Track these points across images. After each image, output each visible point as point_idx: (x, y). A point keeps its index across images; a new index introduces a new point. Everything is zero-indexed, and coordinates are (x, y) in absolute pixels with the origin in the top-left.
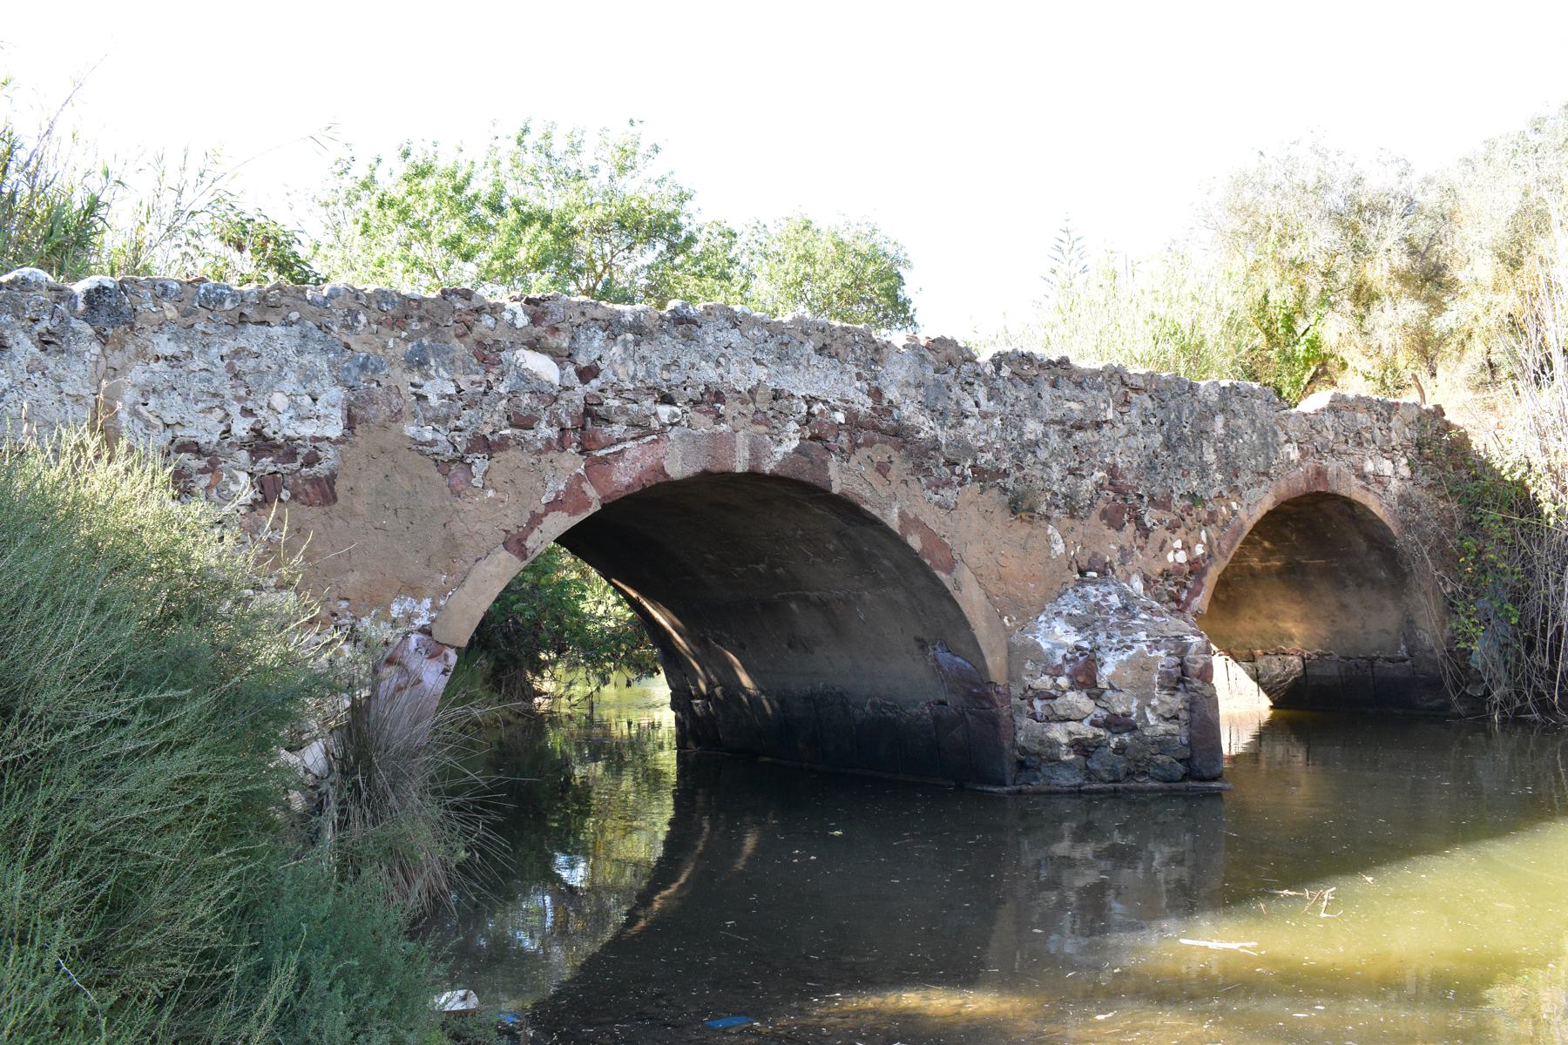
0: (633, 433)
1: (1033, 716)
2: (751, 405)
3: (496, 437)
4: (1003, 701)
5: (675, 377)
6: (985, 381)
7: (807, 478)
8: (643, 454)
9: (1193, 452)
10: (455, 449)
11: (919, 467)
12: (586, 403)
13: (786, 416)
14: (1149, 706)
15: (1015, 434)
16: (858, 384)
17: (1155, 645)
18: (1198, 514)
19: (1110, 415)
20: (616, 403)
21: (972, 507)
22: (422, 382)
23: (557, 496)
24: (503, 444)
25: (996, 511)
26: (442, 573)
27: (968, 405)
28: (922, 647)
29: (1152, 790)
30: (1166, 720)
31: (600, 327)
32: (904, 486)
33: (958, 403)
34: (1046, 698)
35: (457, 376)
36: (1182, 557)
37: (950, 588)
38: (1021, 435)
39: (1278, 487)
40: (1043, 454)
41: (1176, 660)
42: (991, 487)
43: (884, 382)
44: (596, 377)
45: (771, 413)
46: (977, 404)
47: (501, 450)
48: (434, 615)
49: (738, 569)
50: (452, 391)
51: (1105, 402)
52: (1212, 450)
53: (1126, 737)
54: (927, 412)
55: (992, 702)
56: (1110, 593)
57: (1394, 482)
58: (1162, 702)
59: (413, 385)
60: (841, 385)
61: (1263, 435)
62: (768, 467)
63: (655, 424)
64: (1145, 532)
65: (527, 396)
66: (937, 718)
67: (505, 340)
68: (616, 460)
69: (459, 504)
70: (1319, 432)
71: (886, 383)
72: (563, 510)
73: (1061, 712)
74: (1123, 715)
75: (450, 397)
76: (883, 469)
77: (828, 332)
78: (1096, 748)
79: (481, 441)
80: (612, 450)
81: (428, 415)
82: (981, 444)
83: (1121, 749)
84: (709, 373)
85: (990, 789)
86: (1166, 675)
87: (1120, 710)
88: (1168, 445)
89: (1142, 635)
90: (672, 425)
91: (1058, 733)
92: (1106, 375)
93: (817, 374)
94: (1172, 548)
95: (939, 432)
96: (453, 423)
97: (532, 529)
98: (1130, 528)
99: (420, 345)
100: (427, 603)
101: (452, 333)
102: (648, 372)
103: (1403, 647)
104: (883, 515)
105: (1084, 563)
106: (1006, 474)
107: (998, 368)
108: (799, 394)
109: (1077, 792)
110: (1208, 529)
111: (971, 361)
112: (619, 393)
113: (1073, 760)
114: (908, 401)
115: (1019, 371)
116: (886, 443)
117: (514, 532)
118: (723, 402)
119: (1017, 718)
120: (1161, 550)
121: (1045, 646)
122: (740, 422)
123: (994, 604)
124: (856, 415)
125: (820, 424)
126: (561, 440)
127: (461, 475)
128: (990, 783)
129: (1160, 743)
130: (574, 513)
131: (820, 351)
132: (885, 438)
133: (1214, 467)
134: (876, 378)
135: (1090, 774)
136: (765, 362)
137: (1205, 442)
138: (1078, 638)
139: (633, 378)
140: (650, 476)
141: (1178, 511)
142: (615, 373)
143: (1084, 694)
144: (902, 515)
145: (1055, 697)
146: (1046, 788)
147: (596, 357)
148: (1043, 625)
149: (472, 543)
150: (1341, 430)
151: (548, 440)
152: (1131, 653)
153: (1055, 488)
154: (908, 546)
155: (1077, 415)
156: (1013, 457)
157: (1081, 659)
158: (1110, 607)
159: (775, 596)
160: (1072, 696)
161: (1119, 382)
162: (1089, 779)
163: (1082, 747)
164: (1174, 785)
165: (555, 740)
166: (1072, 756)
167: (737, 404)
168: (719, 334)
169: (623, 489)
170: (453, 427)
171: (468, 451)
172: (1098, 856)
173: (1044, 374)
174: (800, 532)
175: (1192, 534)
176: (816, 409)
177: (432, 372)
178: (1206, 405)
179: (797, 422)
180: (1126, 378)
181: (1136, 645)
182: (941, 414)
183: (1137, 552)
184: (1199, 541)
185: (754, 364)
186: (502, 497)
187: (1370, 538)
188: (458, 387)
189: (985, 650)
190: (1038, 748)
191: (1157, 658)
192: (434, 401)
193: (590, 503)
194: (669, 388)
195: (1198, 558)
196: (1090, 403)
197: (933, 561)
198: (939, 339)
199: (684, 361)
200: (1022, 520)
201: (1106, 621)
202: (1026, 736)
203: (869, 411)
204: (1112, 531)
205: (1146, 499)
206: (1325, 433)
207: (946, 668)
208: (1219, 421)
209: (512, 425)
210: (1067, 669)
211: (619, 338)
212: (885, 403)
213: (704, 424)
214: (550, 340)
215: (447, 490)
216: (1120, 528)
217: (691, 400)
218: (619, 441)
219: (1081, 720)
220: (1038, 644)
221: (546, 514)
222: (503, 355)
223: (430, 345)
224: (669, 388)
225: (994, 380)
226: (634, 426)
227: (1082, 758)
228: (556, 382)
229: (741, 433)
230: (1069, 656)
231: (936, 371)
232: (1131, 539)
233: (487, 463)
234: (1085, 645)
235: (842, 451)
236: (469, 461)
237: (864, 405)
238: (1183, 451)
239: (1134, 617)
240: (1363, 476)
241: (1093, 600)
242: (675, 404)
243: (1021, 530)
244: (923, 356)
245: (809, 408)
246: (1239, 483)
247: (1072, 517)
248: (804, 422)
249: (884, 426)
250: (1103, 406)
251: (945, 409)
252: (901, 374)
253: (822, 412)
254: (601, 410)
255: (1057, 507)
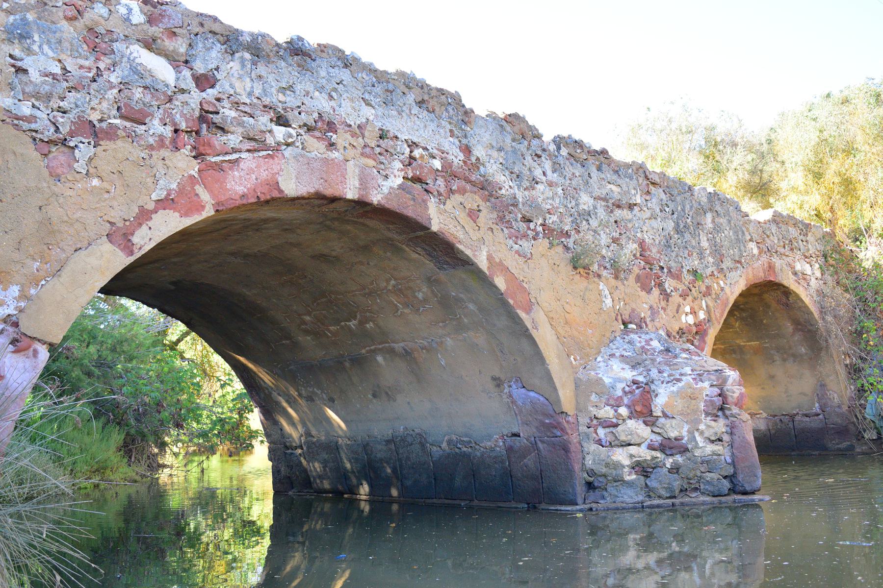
0: (248, 145)
1: (599, 442)
2: (360, 139)
3: (104, 125)
4: (572, 429)
5: (291, 100)
6: (549, 155)
7: (410, 213)
8: (258, 167)
9: (694, 238)
10: (57, 130)
11: (501, 219)
12: (202, 109)
13: (392, 155)
14: (698, 430)
15: (573, 203)
16: (451, 139)
17: (699, 377)
18: (699, 287)
19: (639, 201)
20: (233, 114)
21: (543, 259)
22: (23, 55)
23: (169, 194)
24: (111, 133)
25: (562, 265)
26: (34, 259)
27: (538, 173)
28: (498, 386)
29: (704, 503)
30: (712, 442)
31: (219, 41)
32: (490, 232)
33: (530, 169)
34: (609, 427)
35: (63, 57)
36: (691, 320)
37: (529, 326)
38: (577, 205)
39: (748, 274)
40: (594, 223)
41: (716, 391)
42: (558, 244)
43: (472, 142)
44: (212, 87)
45: (378, 150)
46: (544, 174)
47: (110, 140)
48: (23, 304)
49: (332, 328)
50: (57, 70)
51: (635, 189)
52: (705, 239)
53: (679, 458)
54: (507, 173)
55: (563, 430)
56: (651, 339)
57: (813, 279)
58: (709, 426)
59: (11, 56)
60: (437, 136)
61: (736, 233)
62: (376, 198)
63: (270, 141)
64: (666, 296)
65: (140, 90)
66: (510, 449)
67: (120, 30)
68: (231, 169)
69: (59, 188)
70: (768, 237)
71: (475, 142)
72: (175, 210)
73: (623, 438)
74: (676, 439)
75: (54, 77)
76: (473, 215)
77: (426, 90)
78: (653, 468)
79: (87, 126)
80: (227, 158)
81: (27, 90)
82: (549, 207)
83: (675, 469)
84: (321, 103)
85: (563, 508)
86: (710, 403)
87: (673, 434)
88: (677, 230)
89: (688, 370)
90: (288, 145)
91: (621, 456)
92: (634, 168)
93: (418, 123)
94: (684, 311)
95: (517, 191)
96: (55, 103)
97: (140, 225)
98: (656, 292)
99: (24, 19)
100: (15, 290)
101: (61, 14)
102: (264, 90)
103: (817, 405)
104: (474, 255)
105: (626, 317)
106: (567, 235)
107: (559, 148)
108: (403, 137)
109: (640, 508)
110: (707, 299)
111: (538, 138)
112: (236, 105)
113: (635, 480)
114: (492, 161)
115: (573, 153)
116: (475, 193)
117: (120, 224)
118: (336, 132)
119: (585, 444)
120: (677, 313)
121: (607, 381)
122: (351, 152)
123: (563, 344)
124: (450, 165)
125: (421, 167)
126: (174, 141)
127: (62, 158)
128: (561, 504)
129: (708, 462)
130: (186, 214)
131: (421, 103)
132: (475, 189)
133: (708, 252)
134: (466, 137)
135: (649, 492)
136: (373, 103)
137: (700, 232)
138: (634, 373)
139: (250, 94)
140: (265, 189)
141: (687, 283)
142: (232, 86)
143: (641, 422)
144: (490, 258)
145: (616, 426)
146: (614, 505)
147: (213, 66)
148: (602, 364)
149: (72, 231)
150: (781, 237)
151: (161, 138)
152: (680, 385)
153: (604, 252)
154: (496, 287)
155: (617, 196)
156: (572, 222)
157: (637, 391)
158: (654, 349)
159: (364, 351)
160: (631, 424)
161: (643, 175)
162: (649, 496)
163: (643, 469)
164: (723, 499)
165: (175, 501)
166: (634, 477)
167: (348, 136)
168: (331, 70)
169: (237, 197)
170: (55, 106)
171: (72, 134)
172: (660, 562)
173: (591, 160)
174: (393, 282)
175: (696, 302)
176: (417, 153)
177: (35, 48)
178: (700, 204)
179: (402, 162)
180: (647, 173)
181: (684, 378)
182: (518, 176)
183: (662, 312)
184: (701, 308)
185: (364, 104)
186: (108, 187)
187: (797, 323)
188: (64, 68)
189: (558, 385)
190: (604, 470)
191: (702, 389)
192: (34, 75)
193: (203, 207)
194: (285, 109)
195: (700, 322)
196: (625, 188)
197: (515, 301)
198: (514, 115)
199: (298, 87)
200: (581, 276)
201: (653, 360)
202: (594, 460)
203: (461, 163)
204: (644, 293)
205: (665, 270)
206: (771, 237)
207: (520, 403)
208: (709, 216)
209: (122, 117)
210: (626, 401)
211: (237, 55)
212: (473, 159)
213: (316, 147)
214: (167, 43)
215: (46, 173)
216: (649, 291)
217: (305, 125)
218: (235, 151)
219: (639, 445)
220: (601, 379)
221: (155, 211)
222: (115, 46)
223: (35, 22)
224: (285, 109)
225: (556, 157)
226: (250, 139)
227: (642, 478)
228: (172, 83)
229: (351, 163)
230: (627, 389)
231: (514, 140)
232: (657, 301)
233: (93, 150)
234: (641, 379)
235: (440, 194)
236: (72, 144)
237: (457, 157)
238: (687, 236)
239: (676, 357)
240: (795, 274)
241: (638, 345)
242: (290, 126)
243: (581, 284)
244: (502, 126)
245: (411, 152)
246: (724, 266)
247: (616, 277)
248: (407, 163)
249: (473, 178)
250: (633, 192)
251: (521, 173)
252: (486, 138)
253: (422, 157)
254: (216, 119)
255: (605, 268)
